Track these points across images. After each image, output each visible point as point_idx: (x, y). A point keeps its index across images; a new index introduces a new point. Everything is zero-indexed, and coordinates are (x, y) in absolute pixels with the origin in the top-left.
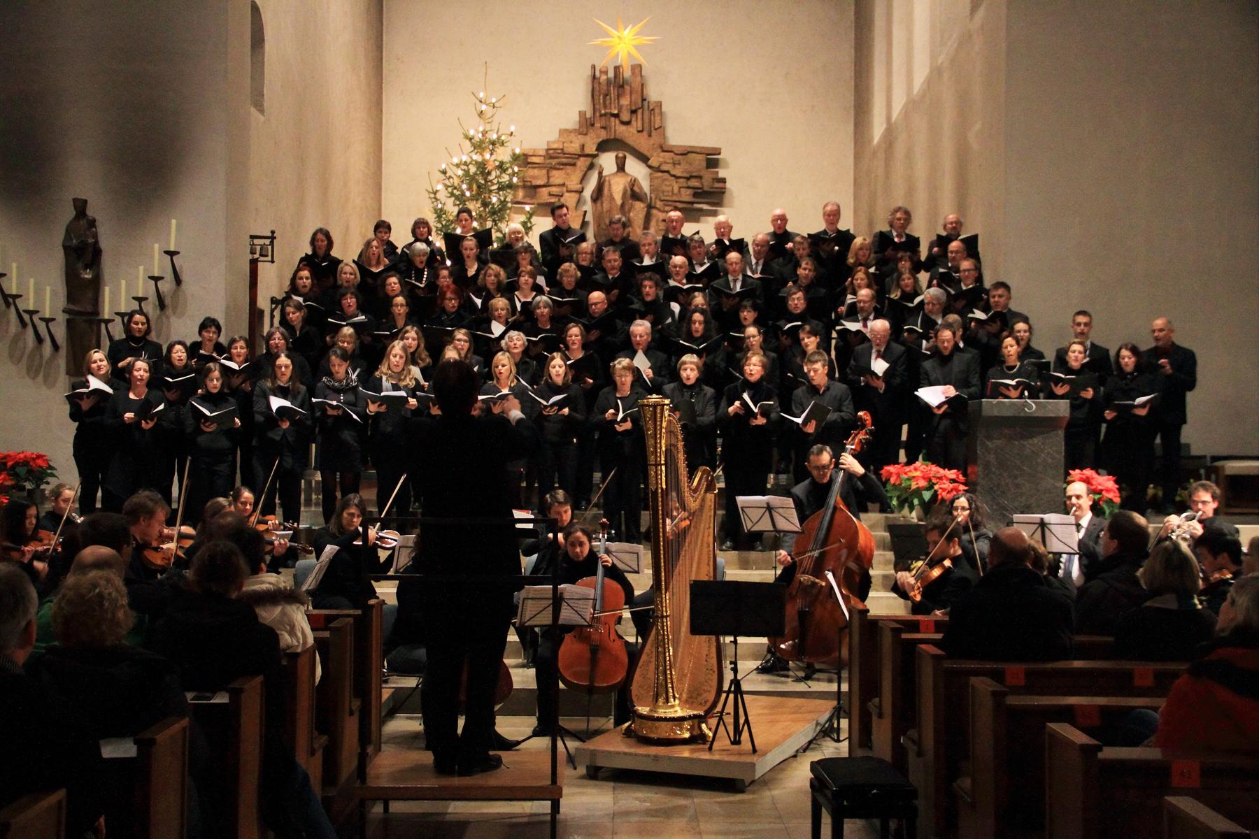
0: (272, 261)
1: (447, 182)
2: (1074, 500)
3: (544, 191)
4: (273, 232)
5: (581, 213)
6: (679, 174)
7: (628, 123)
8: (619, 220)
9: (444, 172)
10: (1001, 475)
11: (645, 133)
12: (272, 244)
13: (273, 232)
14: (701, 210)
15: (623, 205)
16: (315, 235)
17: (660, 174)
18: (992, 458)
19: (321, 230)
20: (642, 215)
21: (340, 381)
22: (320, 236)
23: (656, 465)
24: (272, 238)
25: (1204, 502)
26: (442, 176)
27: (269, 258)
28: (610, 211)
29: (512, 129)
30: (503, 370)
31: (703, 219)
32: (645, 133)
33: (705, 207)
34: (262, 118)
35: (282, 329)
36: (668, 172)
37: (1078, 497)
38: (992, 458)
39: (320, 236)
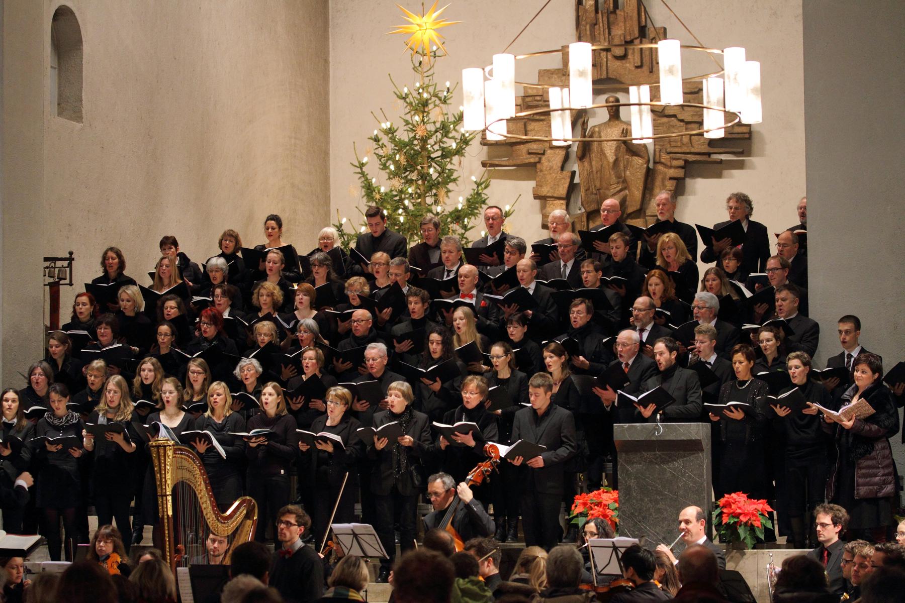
0: (71, 284)
1: (381, 152)
2: (683, 525)
3: (523, 148)
4: (71, 253)
5: (567, 174)
6: (689, 119)
7: (623, 57)
8: (431, 220)
9: (376, 140)
10: (642, 500)
11: (646, 69)
12: (70, 265)
13: (71, 253)
14: (721, 161)
15: (616, 162)
16: (106, 253)
17: (665, 120)
18: (632, 483)
19: (112, 249)
20: (641, 174)
21: (60, 418)
22: (110, 254)
23: (162, 496)
24: (71, 259)
25: (824, 525)
26: (374, 145)
27: (67, 281)
28: (600, 171)
29: (448, 84)
30: (219, 399)
31: (725, 172)
32: (646, 69)
33: (723, 157)
34: (79, 126)
35: (45, 364)
36: (674, 116)
37: (687, 522)
38: (632, 483)
39: (110, 254)
